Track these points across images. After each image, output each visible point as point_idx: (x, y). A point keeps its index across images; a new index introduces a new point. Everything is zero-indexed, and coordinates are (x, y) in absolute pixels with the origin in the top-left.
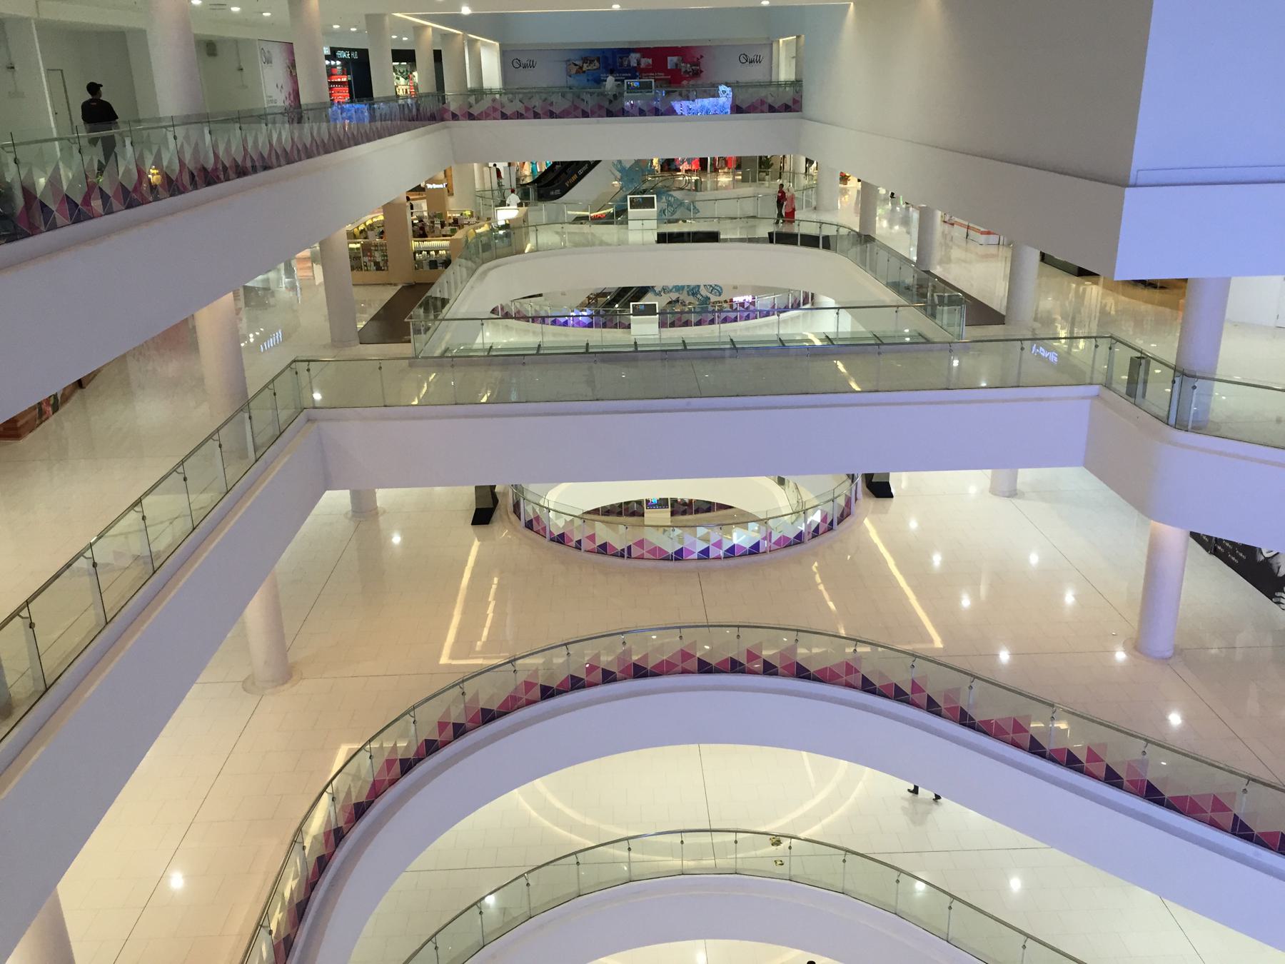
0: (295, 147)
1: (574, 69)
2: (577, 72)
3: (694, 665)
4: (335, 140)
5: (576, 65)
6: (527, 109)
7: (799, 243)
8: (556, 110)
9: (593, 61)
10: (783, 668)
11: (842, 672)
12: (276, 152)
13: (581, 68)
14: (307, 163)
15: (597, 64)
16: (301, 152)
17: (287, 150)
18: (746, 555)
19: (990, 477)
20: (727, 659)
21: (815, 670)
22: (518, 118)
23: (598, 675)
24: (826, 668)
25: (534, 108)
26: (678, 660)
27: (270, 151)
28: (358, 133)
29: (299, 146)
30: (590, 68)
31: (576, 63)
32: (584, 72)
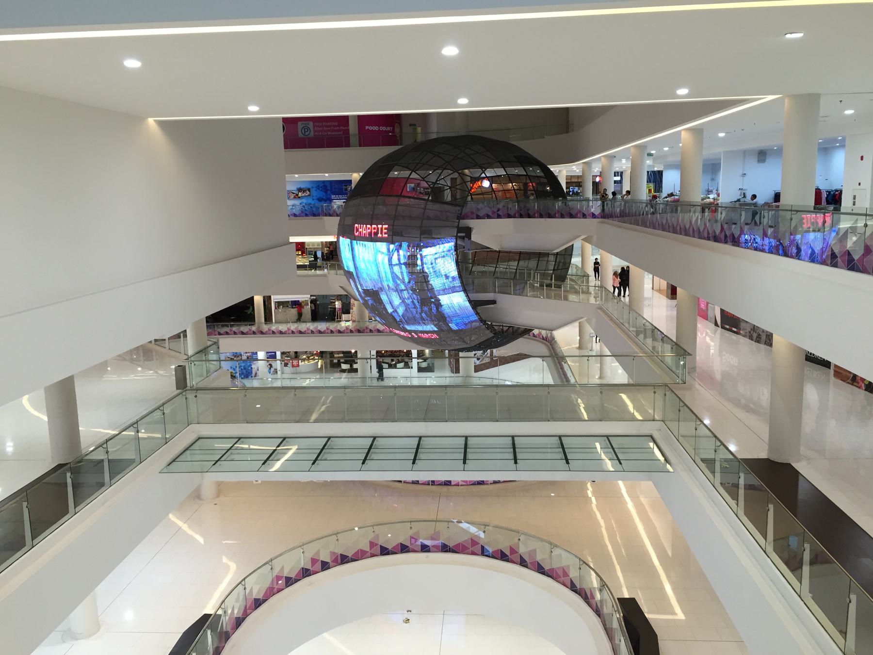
0: (691, 228)
1: (292, 196)
2: (295, 197)
3: (377, 550)
4: (670, 225)
5: (293, 193)
6: (493, 212)
7: (563, 299)
8: (481, 214)
9: (306, 191)
10: (530, 563)
11: (469, 545)
12: (708, 231)
13: (297, 195)
14: (711, 243)
15: (308, 193)
16: (695, 232)
17: (700, 229)
18: (475, 484)
19: (767, 443)
20: (399, 544)
21: (453, 545)
22: (498, 218)
23: (318, 566)
24: (460, 543)
25: (498, 211)
26: (367, 548)
27: (704, 229)
28: (666, 223)
29: (709, 229)
30: (303, 195)
31: (294, 192)
32: (299, 197)
